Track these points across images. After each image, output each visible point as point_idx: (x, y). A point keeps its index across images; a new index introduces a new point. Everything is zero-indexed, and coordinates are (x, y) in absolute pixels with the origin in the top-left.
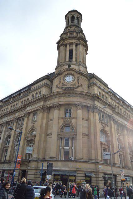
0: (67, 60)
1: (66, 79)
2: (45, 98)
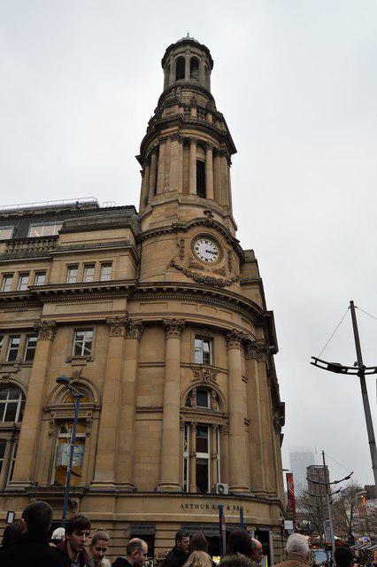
0: (194, 190)
1: (197, 249)
2: (134, 293)
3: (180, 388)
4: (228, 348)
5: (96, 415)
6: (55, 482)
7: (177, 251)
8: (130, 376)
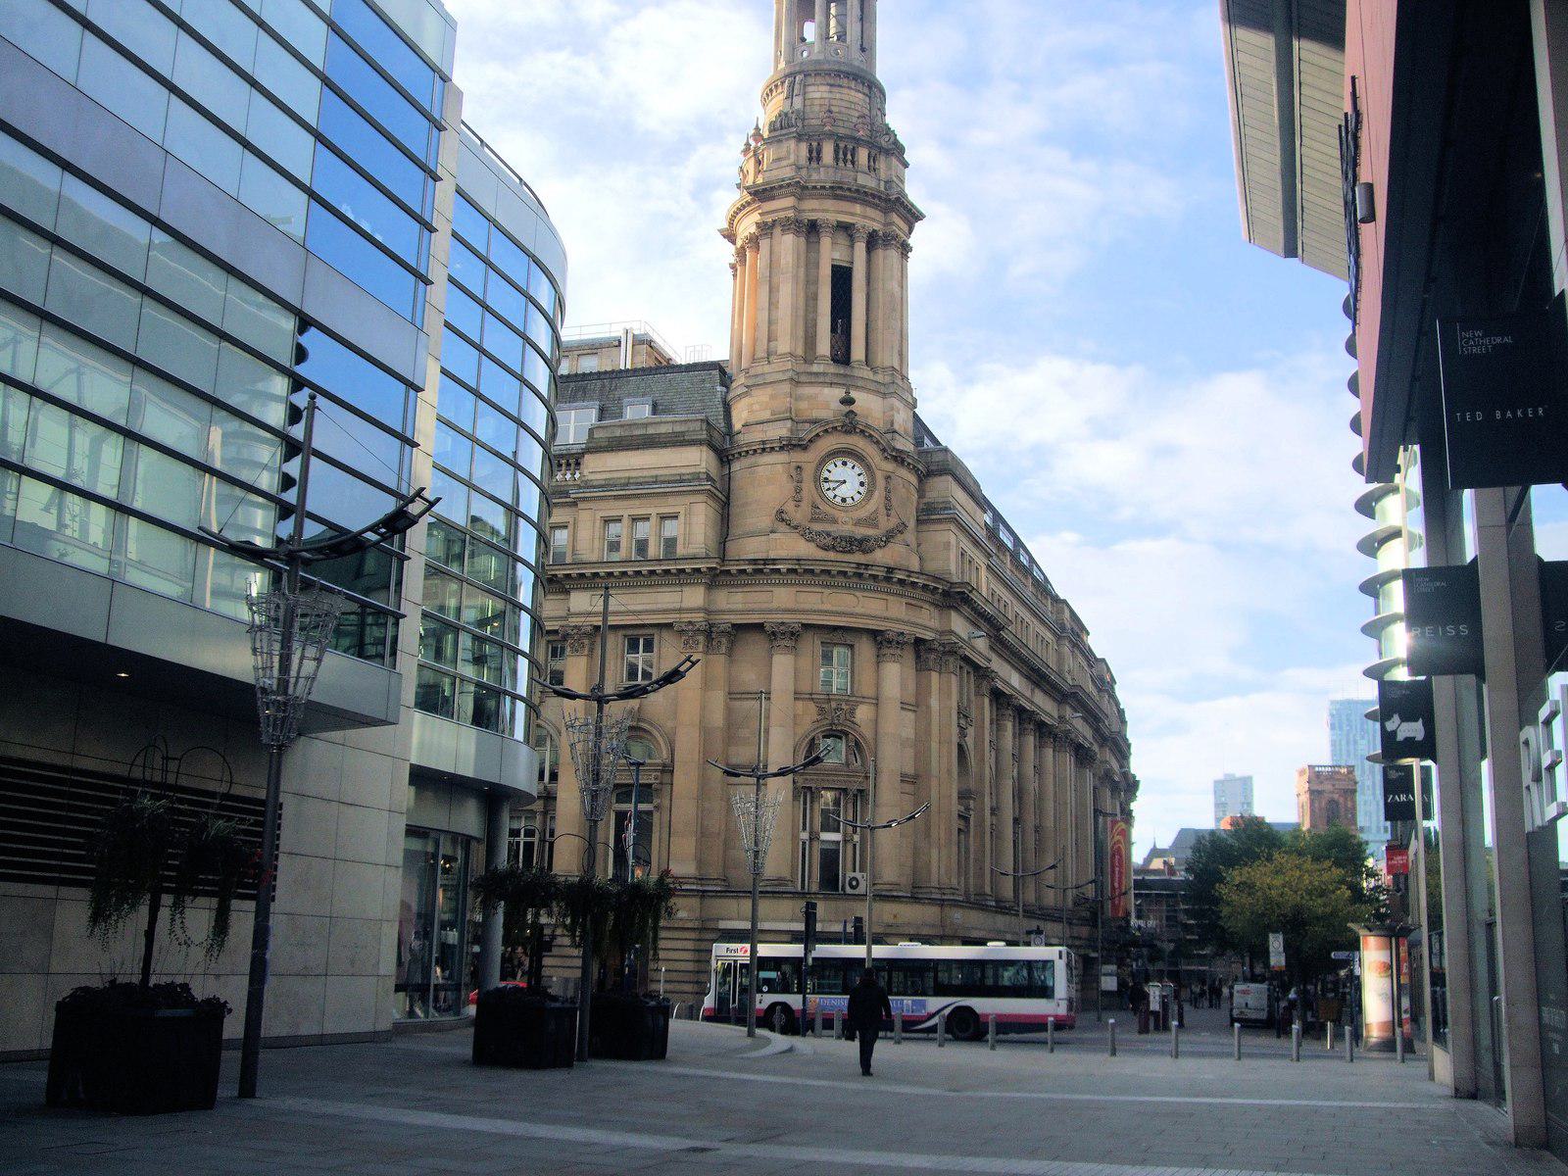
0: (824, 346)
3: (795, 734)
4: (879, 659)
5: (666, 778)
6: (614, 875)
7: (789, 487)
8: (717, 718)
